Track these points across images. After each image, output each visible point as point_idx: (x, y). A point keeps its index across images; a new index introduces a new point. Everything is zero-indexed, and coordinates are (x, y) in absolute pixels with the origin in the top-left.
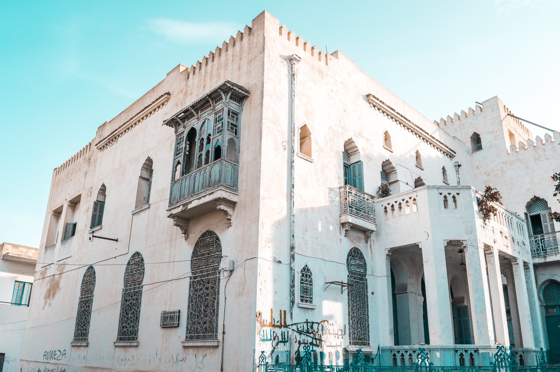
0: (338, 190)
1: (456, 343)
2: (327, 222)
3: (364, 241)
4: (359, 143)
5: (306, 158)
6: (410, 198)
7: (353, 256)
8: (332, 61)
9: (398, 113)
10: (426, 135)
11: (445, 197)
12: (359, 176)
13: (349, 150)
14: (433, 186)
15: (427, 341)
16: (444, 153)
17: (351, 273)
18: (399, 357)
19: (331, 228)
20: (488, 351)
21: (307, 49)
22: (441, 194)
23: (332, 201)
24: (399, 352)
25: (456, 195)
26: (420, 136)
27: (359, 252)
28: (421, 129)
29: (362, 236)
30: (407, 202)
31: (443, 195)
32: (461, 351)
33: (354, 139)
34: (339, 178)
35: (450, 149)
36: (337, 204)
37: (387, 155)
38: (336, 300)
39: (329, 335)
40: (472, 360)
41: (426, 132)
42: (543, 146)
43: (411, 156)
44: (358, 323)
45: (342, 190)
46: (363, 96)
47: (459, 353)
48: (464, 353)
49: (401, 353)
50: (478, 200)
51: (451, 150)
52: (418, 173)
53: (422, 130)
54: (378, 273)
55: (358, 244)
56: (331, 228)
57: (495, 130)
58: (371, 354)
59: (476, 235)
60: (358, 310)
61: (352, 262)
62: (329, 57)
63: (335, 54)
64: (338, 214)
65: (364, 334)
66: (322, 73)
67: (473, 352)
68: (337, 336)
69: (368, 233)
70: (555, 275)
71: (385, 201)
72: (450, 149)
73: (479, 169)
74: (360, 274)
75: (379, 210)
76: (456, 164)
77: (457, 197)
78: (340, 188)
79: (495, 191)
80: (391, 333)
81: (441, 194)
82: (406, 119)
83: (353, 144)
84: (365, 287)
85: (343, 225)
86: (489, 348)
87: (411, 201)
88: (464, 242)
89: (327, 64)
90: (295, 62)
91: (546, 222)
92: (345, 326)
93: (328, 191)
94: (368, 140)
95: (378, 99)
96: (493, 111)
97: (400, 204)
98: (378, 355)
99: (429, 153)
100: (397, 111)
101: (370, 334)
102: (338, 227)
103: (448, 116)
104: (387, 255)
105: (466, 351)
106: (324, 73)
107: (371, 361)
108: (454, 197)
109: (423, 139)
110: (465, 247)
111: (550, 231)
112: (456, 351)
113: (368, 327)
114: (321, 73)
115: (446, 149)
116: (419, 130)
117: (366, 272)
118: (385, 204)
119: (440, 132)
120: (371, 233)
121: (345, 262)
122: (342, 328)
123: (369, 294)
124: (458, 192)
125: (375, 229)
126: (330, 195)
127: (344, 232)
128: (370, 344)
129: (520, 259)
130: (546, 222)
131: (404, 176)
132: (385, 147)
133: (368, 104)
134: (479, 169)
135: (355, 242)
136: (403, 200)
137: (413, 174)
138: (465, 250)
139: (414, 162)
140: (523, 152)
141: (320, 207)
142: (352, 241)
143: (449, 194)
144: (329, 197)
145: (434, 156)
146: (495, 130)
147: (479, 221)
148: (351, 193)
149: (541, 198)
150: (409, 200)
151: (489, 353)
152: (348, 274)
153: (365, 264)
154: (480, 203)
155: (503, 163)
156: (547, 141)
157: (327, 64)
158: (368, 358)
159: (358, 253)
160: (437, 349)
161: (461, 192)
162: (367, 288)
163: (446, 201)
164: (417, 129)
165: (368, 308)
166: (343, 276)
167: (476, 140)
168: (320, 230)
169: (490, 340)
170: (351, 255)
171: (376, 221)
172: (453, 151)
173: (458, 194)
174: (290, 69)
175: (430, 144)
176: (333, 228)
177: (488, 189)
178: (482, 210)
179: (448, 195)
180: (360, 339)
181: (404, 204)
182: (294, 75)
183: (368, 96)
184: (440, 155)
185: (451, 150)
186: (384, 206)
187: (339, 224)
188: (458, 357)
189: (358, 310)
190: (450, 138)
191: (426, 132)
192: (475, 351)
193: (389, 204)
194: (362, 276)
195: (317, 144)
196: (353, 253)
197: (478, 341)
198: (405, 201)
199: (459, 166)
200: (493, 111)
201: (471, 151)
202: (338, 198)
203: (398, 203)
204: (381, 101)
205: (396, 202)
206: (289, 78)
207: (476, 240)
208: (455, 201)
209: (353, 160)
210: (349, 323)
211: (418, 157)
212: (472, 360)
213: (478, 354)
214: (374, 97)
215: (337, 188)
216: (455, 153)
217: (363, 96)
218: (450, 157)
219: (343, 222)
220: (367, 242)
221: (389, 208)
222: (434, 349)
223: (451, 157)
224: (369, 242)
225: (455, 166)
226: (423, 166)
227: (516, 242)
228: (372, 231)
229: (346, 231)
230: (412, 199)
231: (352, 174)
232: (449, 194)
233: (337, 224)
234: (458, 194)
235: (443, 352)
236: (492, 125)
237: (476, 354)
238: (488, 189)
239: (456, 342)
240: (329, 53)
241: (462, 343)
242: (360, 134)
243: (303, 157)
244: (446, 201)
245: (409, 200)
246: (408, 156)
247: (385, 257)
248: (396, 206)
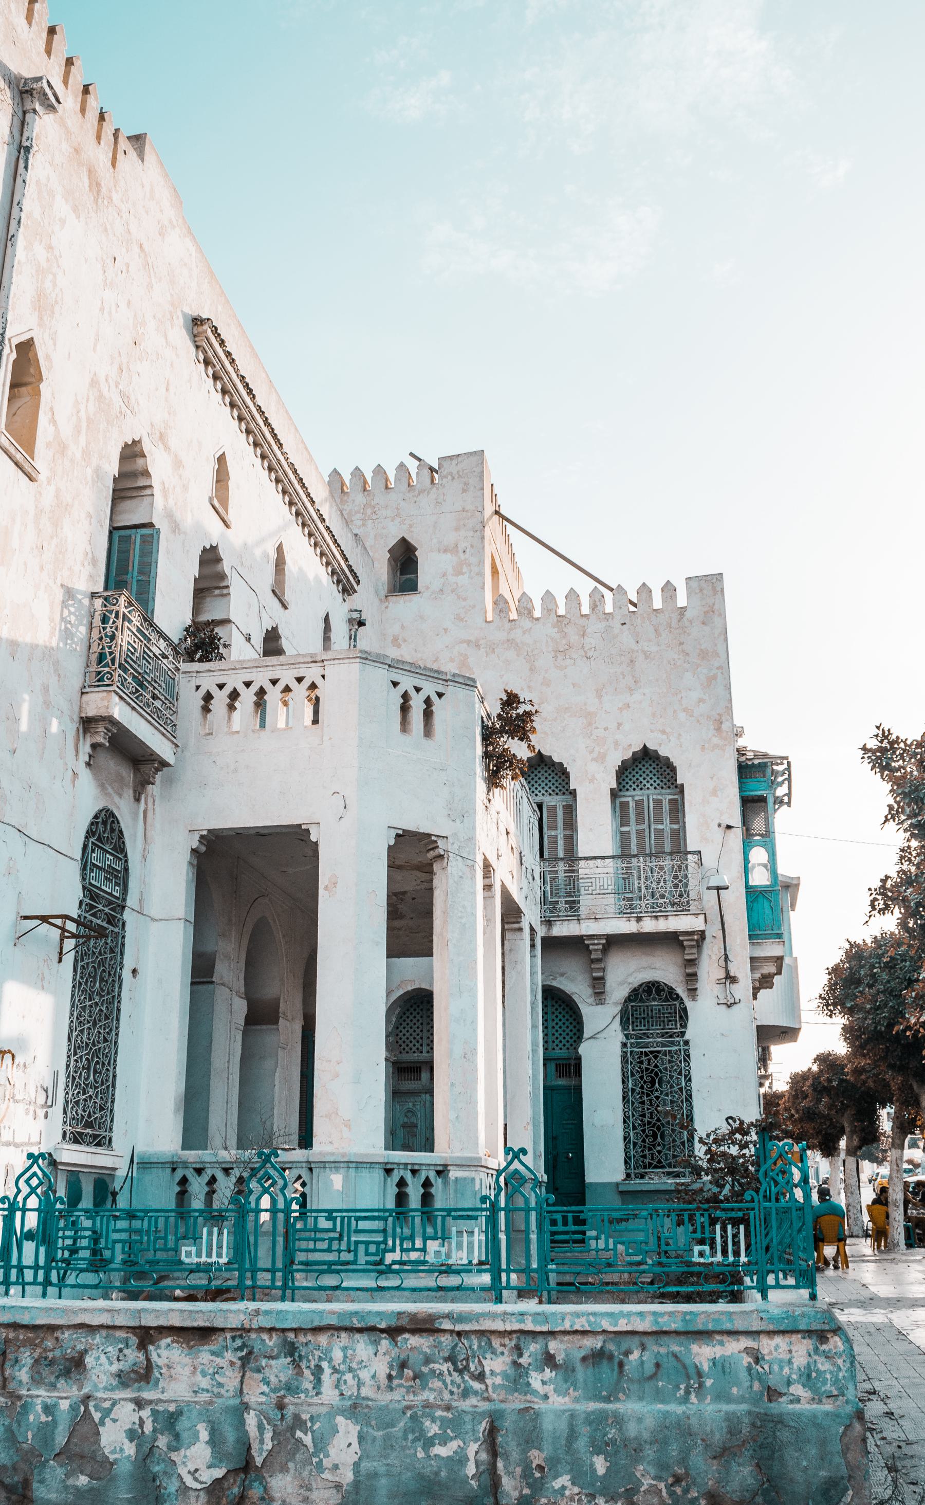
0: (86, 602)
1: (386, 1149)
2: (47, 704)
3: (131, 792)
4: (158, 465)
5: (18, 457)
6: (299, 680)
7: (99, 839)
8: (128, 161)
9: (259, 409)
10: (308, 504)
11: (405, 696)
12: (140, 572)
13: (130, 479)
14: (378, 655)
15: (306, 1140)
16: (333, 573)
17: (91, 893)
18: (198, 1186)
19: (55, 727)
20: (473, 1174)
21: (71, 81)
22: (395, 684)
23: (67, 635)
24: (199, 1171)
25: (434, 698)
26: (291, 504)
27: (115, 826)
28: (300, 480)
29: (128, 775)
30: (287, 689)
31: (401, 689)
32: (402, 1173)
33: (147, 447)
34: (94, 562)
35: (350, 567)
36: (80, 648)
37: (214, 532)
38: (41, 983)
39: (12, 1104)
40: (427, 1198)
41: (308, 495)
42: (583, 621)
43: (266, 556)
44: (88, 1069)
45: (98, 603)
46: (185, 315)
47: (396, 1177)
48: (408, 1177)
49: (236, 1173)
50: (484, 727)
51: (352, 571)
52: (274, 615)
53: (303, 486)
54: (154, 908)
55: (116, 799)
56: (55, 727)
57: (462, 546)
58: (112, 1176)
59: (474, 828)
60: (95, 1024)
61: (95, 857)
62: (123, 144)
63: (138, 140)
64: (76, 683)
65: (102, 1109)
66: (98, 185)
67: (432, 1175)
68: (32, 1108)
69: (145, 768)
70: (562, 975)
71: (206, 676)
72: (350, 567)
73: (399, 646)
74: (111, 903)
75: (190, 701)
76: (355, 615)
77: (438, 706)
78: (94, 595)
79: (528, 708)
80: (177, 1110)
81: (395, 684)
82: (275, 436)
83: (140, 461)
84: (117, 949)
85: (87, 724)
86: (475, 1164)
87: (300, 691)
88: (440, 843)
89: (114, 165)
90: (38, 107)
91: (556, 828)
92: (56, 1074)
93: (59, 595)
94: (178, 464)
95: (222, 343)
96: (464, 491)
97: (261, 692)
98: (129, 1179)
99: (305, 563)
100: (259, 400)
101: (115, 1109)
102: (72, 727)
103: (357, 469)
104: (194, 851)
105: (414, 1172)
106: (104, 190)
107: (110, 1198)
108: (428, 701)
109: (298, 514)
110: (441, 857)
111: (561, 854)
112: (388, 1171)
113: (114, 1086)
114: (95, 185)
115: (342, 562)
116: (295, 482)
117: (124, 900)
118: (208, 683)
119: (331, 506)
120: (157, 770)
121: (78, 856)
122: (49, 1084)
123: (126, 974)
124: (441, 689)
125: (172, 762)
126: (66, 613)
127: (88, 749)
128: (114, 1144)
129: (527, 916)
130: (556, 828)
131: (245, 612)
132: (216, 503)
133: (193, 349)
134: (399, 646)
135: (110, 790)
136: (274, 682)
137: (264, 615)
138: (436, 867)
139: (267, 577)
140: (526, 623)
141: (34, 647)
142: (102, 787)
143: (418, 690)
144: (63, 619)
145: (311, 576)
146: (462, 546)
147: (481, 786)
148: (130, 621)
149: (556, 759)
150: (293, 684)
151: (473, 1180)
152: (81, 895)
153: (126, 870)
154: (488, 735)
155: (469, 642)
156: (594, 607)
157: (114, 165)
158: (104, 1187)
159: (112, 830)
160: (335, 1165)
161: (451, 691)
162: (122, 954)
163: (405, 708)
164: (292, 477)
165: (118, 1020)
166: (69, 899)
167: (404, 563)
168: (24, 726)
169: (479, 1142)
170: (94, 834)
171: (178, 734)
172: (355, 577)
173: (440, 695)
174: (17, 123)
175: (310, 535)
176: (60, 726)
177: (511, 700)
178: (487, 755)
179: (412, 692)
180: (89, 1125)
181: (273, 695)
182: (28, 149)
183: (197, 321)
184: (323, 574)
185: (352, 571)
186: (202, 692)
187: (76, 718)
188: (393, 1191)
189: (95, 1024)
190: (350, 535)
191: (308, 495)
192: (439, 1173)
193: (221, 686)
194: (113, 909)
195: (53, 421)
196: (101, 828)
197: (446, 1145)
198: (280, 686)
199: (361, 624)
200: (464, 491)
201: (383, 591)
202: (83, 630)
203: (254, 688)
204: (228, 354)
205: (248, 684)
206: (9, 154)
207: (471, 839)
208: (428, 714)
209: (133, 515)
210: (68, 1066)
211: (280, 563)
212: (427, 1198)
213: (446, 1182)
214: (215, 330)
215: (83, 593)
216: (358, 582)
217: (185, 315)
218: (345, 591)
219: (91, 713)
220: (138, 800)
221: (220, 699)
222: (323, 1164)
223: (347, 590)
224: (143, 801)
225: (350, 621)
226: (288, 597)
227: (524, 867)
228: (164, 764)
229: (94, 746)
230: (306, 683)
231: (128, 558)
232: (418, 690)
233: (72, 719)
234: (440, 695)
235: (352, 1171)
236: (457, 529)
237: (440, 1181)
238: (511, 700)
239: (386, 1149)
240: (126, 132)
241: (407, 1147)
242: (162, 437)
243: (12, 450)
244: (405, 708)
245: (293, 684)
246: (258, 552)
247: (187, 856)
248: (247, 697)
